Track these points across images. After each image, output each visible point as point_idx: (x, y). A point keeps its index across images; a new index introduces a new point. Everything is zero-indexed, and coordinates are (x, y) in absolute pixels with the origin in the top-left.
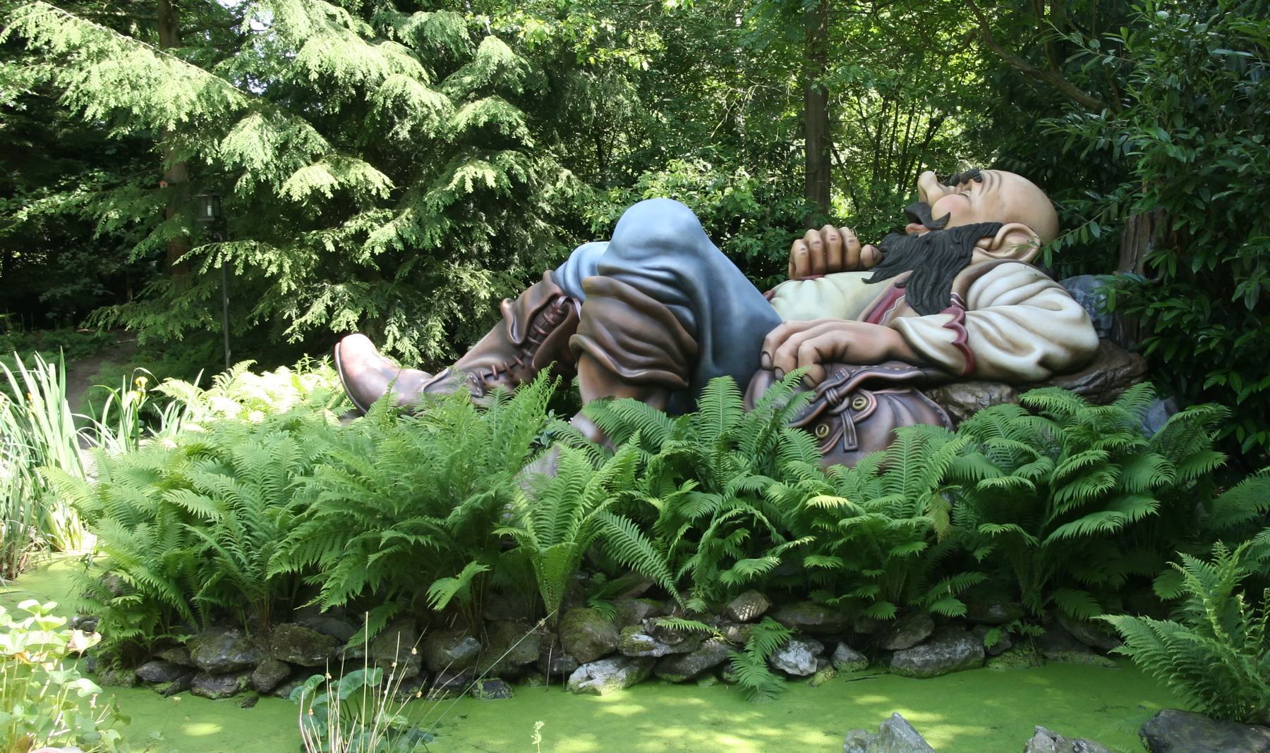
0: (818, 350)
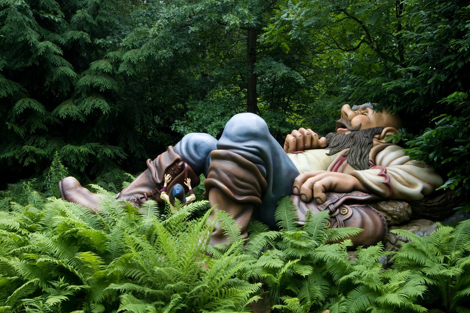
0: (324, 186)
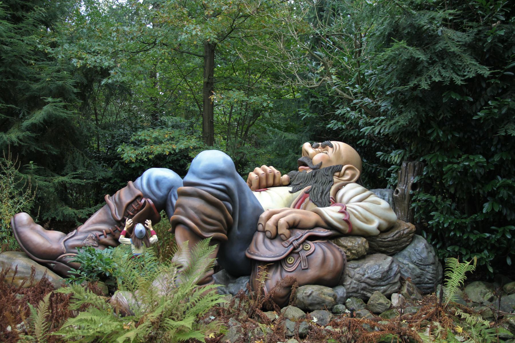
0: (288, 223)
